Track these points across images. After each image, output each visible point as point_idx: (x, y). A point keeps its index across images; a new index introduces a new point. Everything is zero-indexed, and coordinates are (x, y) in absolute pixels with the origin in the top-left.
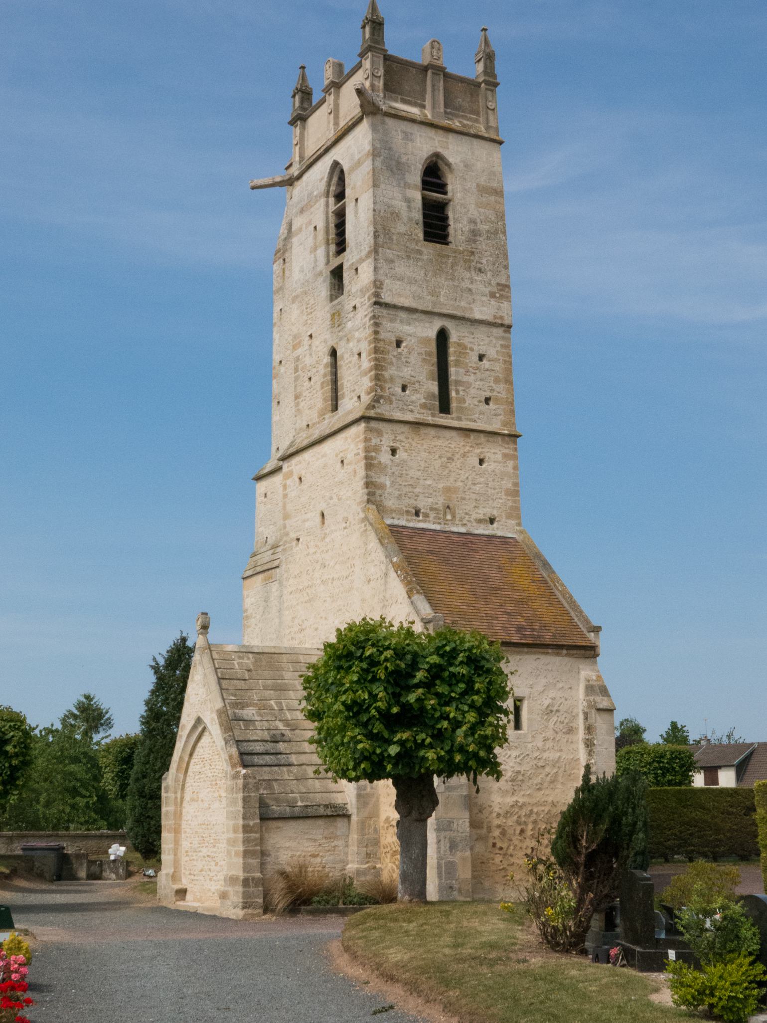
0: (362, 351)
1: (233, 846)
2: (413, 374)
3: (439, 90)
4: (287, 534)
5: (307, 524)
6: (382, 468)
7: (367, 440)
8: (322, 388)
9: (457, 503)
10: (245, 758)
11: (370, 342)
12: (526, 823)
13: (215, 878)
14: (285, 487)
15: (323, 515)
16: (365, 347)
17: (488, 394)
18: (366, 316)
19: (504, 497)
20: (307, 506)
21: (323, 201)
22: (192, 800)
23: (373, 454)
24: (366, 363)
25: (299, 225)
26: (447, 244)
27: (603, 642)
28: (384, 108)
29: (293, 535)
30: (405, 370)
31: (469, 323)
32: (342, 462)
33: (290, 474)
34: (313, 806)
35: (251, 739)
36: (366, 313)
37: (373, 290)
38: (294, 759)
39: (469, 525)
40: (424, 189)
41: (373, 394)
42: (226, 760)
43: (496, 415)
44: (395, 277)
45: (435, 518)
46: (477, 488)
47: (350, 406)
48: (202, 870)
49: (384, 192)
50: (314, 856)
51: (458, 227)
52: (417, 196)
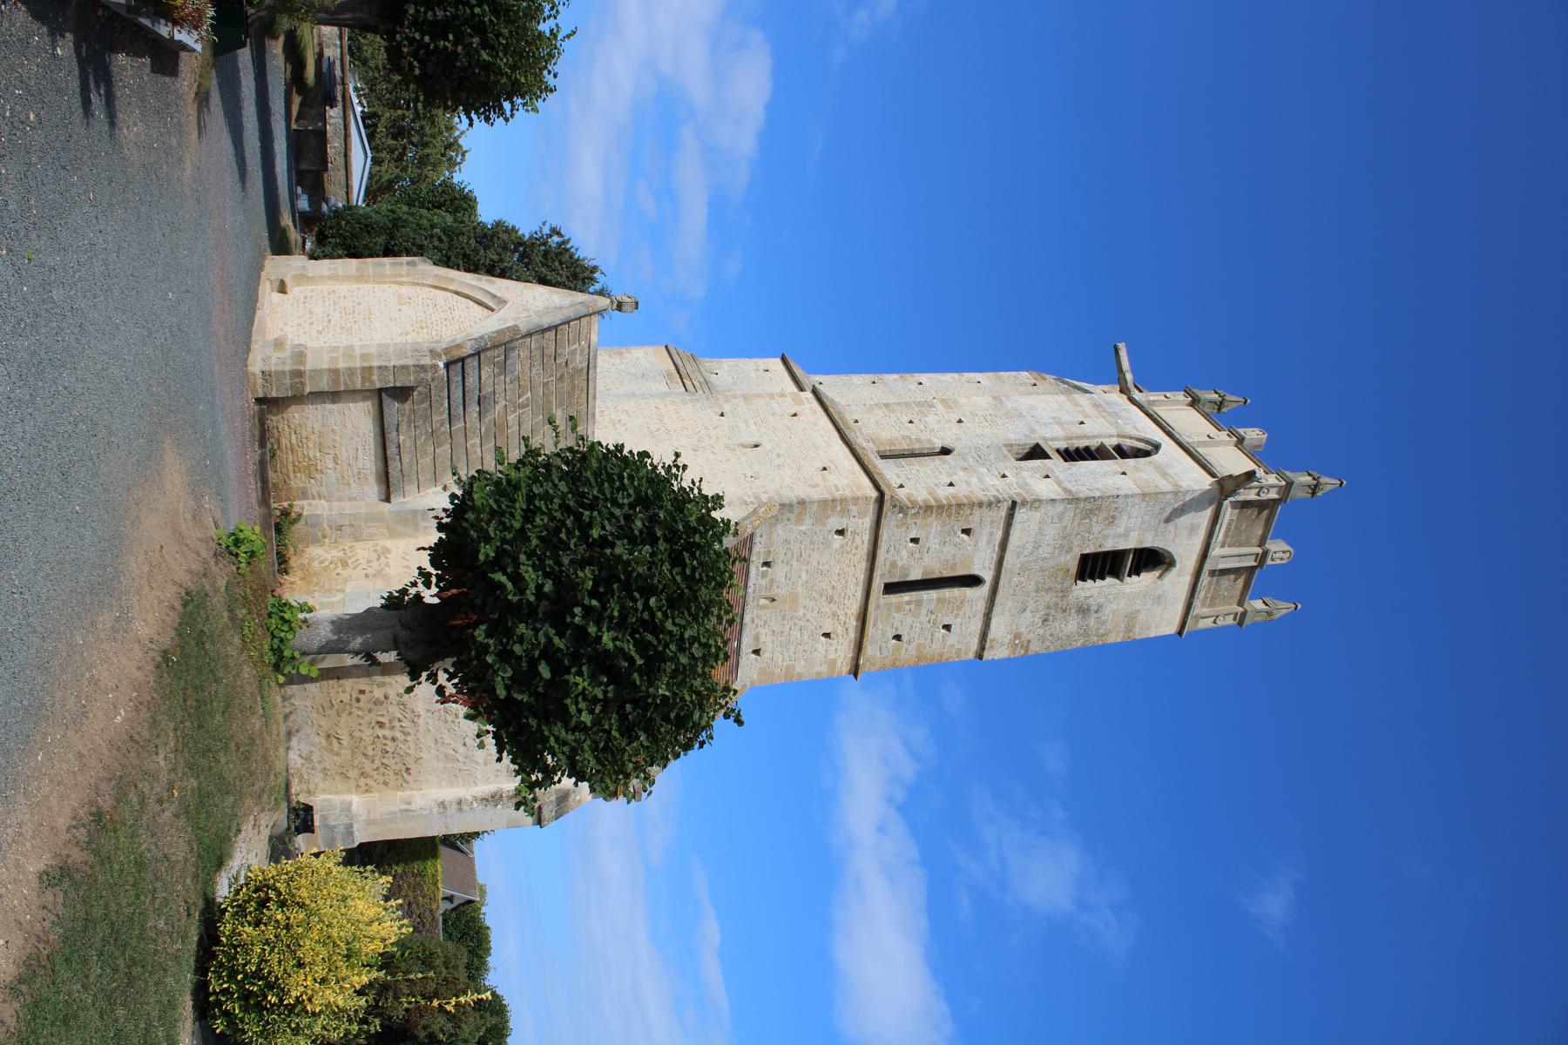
0: (957, 487)
1: (344, 355)
3: (1240, 562)
4: (727, 401)
5: (743, 426)
7: (856, 500)
8: (904, 438)
9: (779, 610)
10: (457, 363)
11: (968, 497)
12: (392, 728)
13: (302, 331)
14: (782, 395)
15: (756, 446)
16: (961, 491)
17: (904, 638)
18: (998, 491)
19: (785, 664)
20: (764, 424)
21: (1113, 431)
22: (400, 297)
23: (839, 508)
24: (944, 493)
29: (726, 408)
30: (936, 541)
31: (987, 611)
32: (825, 469)
34: (400, 455)
35: (482, 372)
36: (1001, 491)
37: (1029, 500)
38: (459, 425)
39: (753, 626)
41: (910, 505)
42: (454, 340)
43: (880, 648)
44: (1042, 523)
46: (796, 633)
47: (901, 478)
48: (311, 313)
49: (1137, 507)
51: (1092, 589)
52: (1131, 543)
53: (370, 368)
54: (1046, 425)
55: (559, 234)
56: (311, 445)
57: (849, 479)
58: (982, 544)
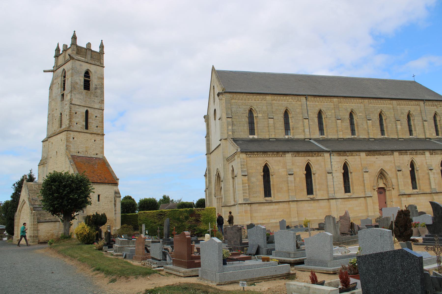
2: (79, 120)
4: (49, 156)
5: (53, 154)
6: (70, 142)
7: (67, 135)
8: (58, 122)
15: (57, 152)
16: (68, 114)
17: (97, 125)
21: (60, 78)
22: (22, 219)
24: (68, 118)
25: (55, 82)
26: (89, 90)
27: (120, 182)
28: (75, 58)
29: (50, 156)
33: (50, 142)
40: (84, 77)
45: (83, 154)
46: (94, 147)
50: (51, 230)
51: (92, 86)
53: (33, 224)
54: (58, 92)
55: (15, 184)
56: (48, 235)
57: (63, 136)
58: (79, 110)
